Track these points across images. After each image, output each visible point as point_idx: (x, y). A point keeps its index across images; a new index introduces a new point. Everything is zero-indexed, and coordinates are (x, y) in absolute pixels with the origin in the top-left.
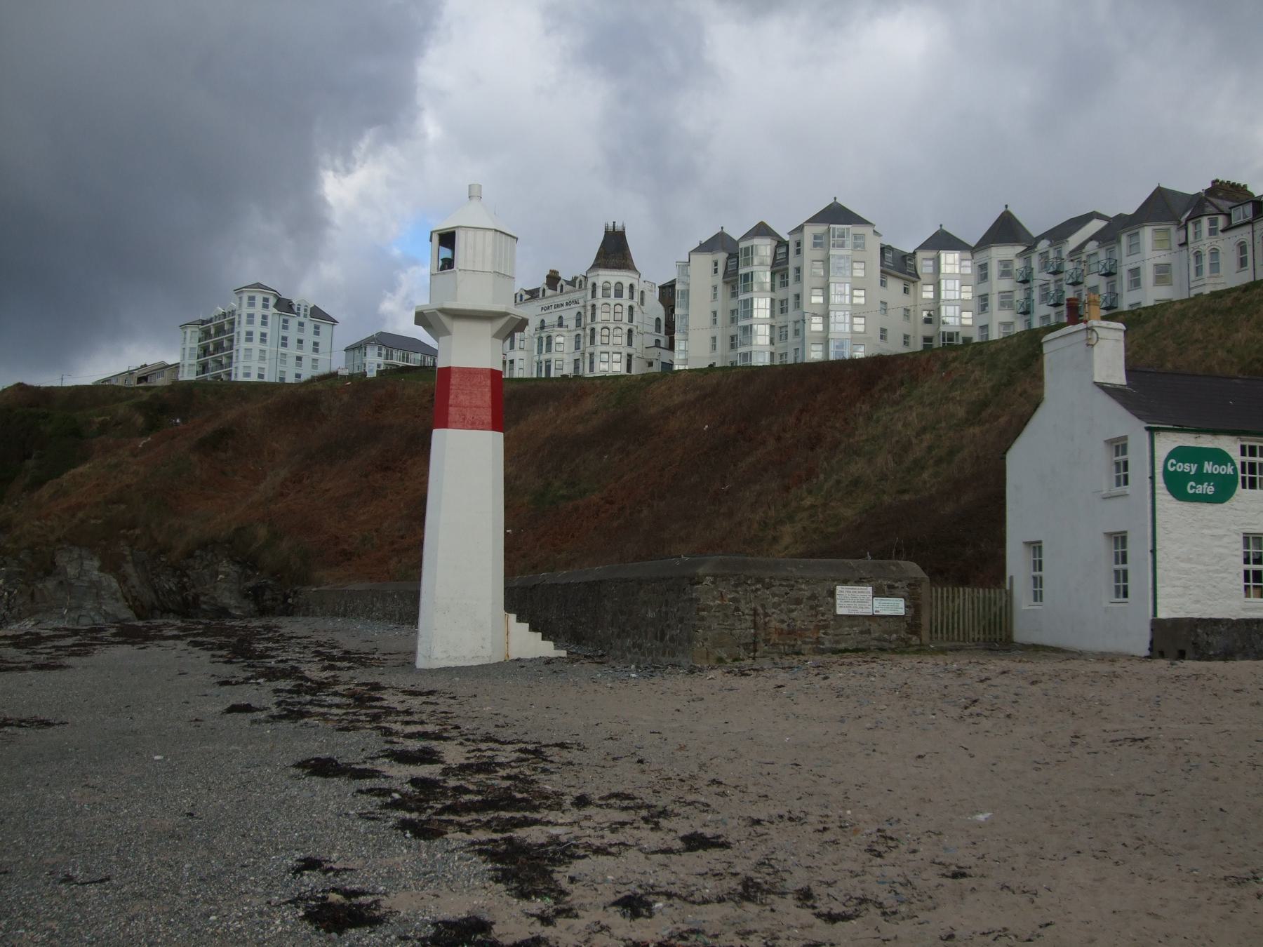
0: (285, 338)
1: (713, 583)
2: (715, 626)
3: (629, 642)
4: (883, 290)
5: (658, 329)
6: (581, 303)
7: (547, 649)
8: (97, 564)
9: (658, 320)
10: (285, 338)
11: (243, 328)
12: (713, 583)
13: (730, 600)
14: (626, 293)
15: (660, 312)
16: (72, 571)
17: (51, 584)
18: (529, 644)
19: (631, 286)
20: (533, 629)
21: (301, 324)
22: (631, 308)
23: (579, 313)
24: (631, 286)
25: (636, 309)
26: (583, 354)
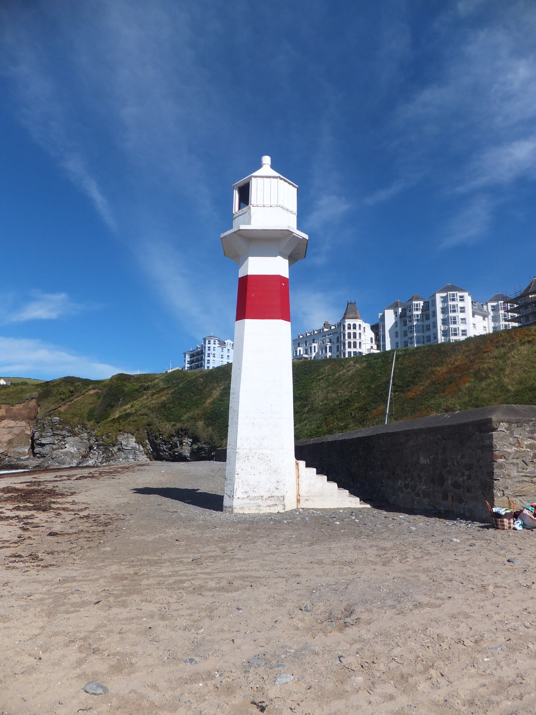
0: (222, 355)
1: (507, 429)
2: (514, 473)
3: (400, 483)
4: (473, 318)
5: (372, 342)
6: (339, 332)
7: (355, 503)
8: (134, 440)
9: (372, 338)
10: (222, 355)
11: (207, 352)
12: (507, 429)
13: (528, 446)
14: (357, 327)
15: (372, 335)
16: (124, 443)
17: (115, 449)
18: (327, 495)
19: (360, 325)
20: (341, 485)
21: (228, 350)
22: (360, 333)
23: (338, 337)
24: (360, 325)
25: (362, 334)
26: (340, 353)
